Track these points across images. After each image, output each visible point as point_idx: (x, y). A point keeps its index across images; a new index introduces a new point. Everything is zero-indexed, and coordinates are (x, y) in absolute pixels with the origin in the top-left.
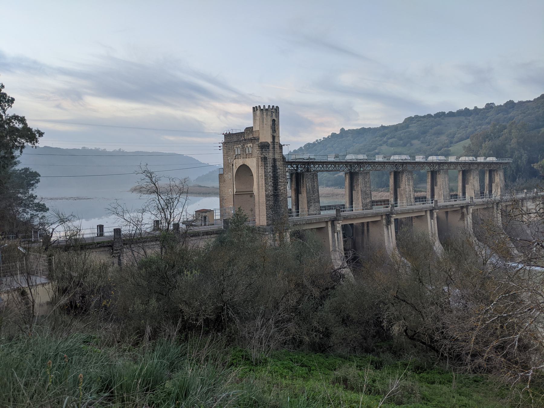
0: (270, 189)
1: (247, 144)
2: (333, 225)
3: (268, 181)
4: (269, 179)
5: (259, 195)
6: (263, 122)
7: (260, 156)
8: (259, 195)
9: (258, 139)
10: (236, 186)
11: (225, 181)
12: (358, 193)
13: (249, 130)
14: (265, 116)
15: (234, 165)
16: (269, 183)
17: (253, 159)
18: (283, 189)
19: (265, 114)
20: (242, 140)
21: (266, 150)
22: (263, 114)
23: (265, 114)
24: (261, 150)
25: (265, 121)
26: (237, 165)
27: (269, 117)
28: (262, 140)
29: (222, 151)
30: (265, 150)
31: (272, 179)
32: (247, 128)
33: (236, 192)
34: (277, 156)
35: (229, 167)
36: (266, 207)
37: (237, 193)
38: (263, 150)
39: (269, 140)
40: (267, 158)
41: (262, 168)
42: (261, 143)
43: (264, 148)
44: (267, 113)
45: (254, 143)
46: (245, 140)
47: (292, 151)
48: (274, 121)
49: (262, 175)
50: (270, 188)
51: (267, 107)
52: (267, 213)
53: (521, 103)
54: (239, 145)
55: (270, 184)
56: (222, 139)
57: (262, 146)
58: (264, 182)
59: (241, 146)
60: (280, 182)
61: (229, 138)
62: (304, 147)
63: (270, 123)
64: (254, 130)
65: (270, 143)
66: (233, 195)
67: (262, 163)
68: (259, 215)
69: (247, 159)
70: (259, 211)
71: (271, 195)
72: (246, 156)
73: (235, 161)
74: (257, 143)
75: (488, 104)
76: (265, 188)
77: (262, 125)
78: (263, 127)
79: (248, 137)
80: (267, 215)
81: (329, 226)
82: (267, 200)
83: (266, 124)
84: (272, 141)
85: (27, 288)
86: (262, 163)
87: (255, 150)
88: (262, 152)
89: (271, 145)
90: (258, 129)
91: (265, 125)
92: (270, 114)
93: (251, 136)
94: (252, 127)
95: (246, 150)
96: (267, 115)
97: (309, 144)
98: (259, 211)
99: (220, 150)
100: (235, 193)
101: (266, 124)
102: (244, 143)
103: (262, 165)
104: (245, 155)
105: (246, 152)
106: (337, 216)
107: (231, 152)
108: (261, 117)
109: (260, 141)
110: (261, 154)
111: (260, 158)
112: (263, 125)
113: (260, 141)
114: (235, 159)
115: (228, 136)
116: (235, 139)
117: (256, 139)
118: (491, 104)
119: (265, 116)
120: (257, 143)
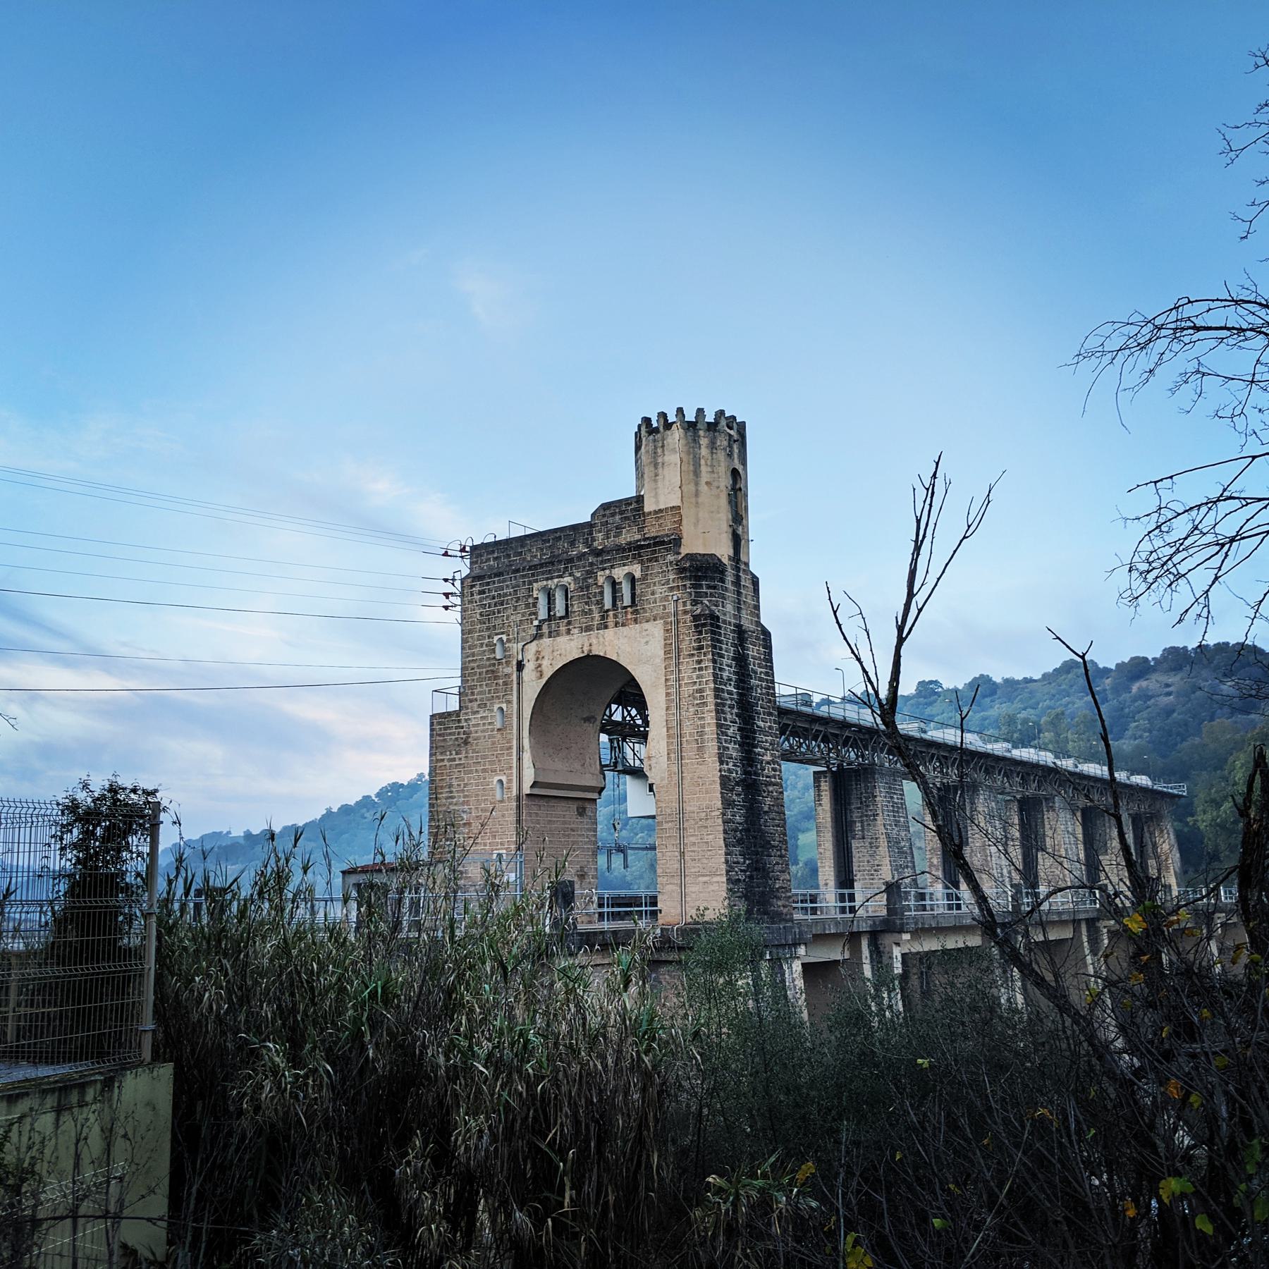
0: (734, 754)
1: (612, 567)
2: (878, 954)
3: (725, 719)
4: (727, 709)
5: (680, 784)
6: (697, 473)
7: (685, 612)
8: (680, 784)
9: (677, 542)
10: (533, 756)
11: (466, 743)
12: (874, 845)
13: (621, 513)
14: (704, 451)
15: (529, 667)
16: (728, 727)
17: (646, 625)
18: (768, 763)
19: (704, 442)
20: (582, 556)
21: (714, 587)
22: (695, 440)
23: (704, 442)
24: (694, 586)
25: (703, 468)
26: (545, 663)
27: (721, 456)
28: (693, 544)
29: (455, 615)
30: (709, 587)
31: (735, 710)
32: (605, 507)
33: (534, 785)
34: (747, 623)
35: (496, 678)
36: (725, 832)
37: (536, 791)
38: (701, 586)
39: (723, 551)
40: (718, 618)
41: (699, 662)
42: (691, 557)
43: (705, 578)
44: (715, 437)
45: (650, 560)
46: (598, 553)
47: (335, 810)
48: (735, 474)
49: (701, 691)
50: (733, 751)
51: (710, 418)
52: (727, 862)
53: (1009, 682)
54: (561, 576)
55: (730, 732)
56: (463, 567)
57: (698, 569)
58: (710, 718)
59: (576, 579)
60: (762, 731)
61: (495, 559)
62: (378, 795)
63: (725, 481)
64: (646, 510)
65: (725, 561)
66: (518, 798)
67: (699, 640)
68: (682, 873)
69: (609, 633)
70: (682, 854)
71: (737, 784)
72: (603, 618)
73: (532, 648)
74: (670, 558)
75: (921, 683)
76: (719, 749)
77: (692, 487)
78: (697, 494)
79: (609, 543)
80: (728, 872)
81: (864, 957)
82: (727, 803)
83: (707, 483)
84: (731, 552)
85: (666, 874)
86: (699, 640)
87: (658, 589)
88: (698, 594)
89: (729, 567)
90: (677, 503)
91: (704, 488)
92: (726, 443)
93: (629, 535)
94: (639, 499)
95: (602, 593)
96: (713, 446)
97: (396, 787)
98: (682, 854)
99: (446, 608)
100: (527, 790)
101: (707, 483)
102: (591, 564)
103: (701, 648)
104: (597, 615)
105: (600, 603)
106: (890, 911)
107: (510, 611)
108: (688, 453)
109: (684, 551)
110: (695, 603)
111: (688, 617)
112: (697, 484)
113: (684, 551)
114: (537, 636)
115: (477, 552)
116: (535, 555)
117: (663, 543)
118: (931, 682)
119: (704, 451)
120: (670, 558)
